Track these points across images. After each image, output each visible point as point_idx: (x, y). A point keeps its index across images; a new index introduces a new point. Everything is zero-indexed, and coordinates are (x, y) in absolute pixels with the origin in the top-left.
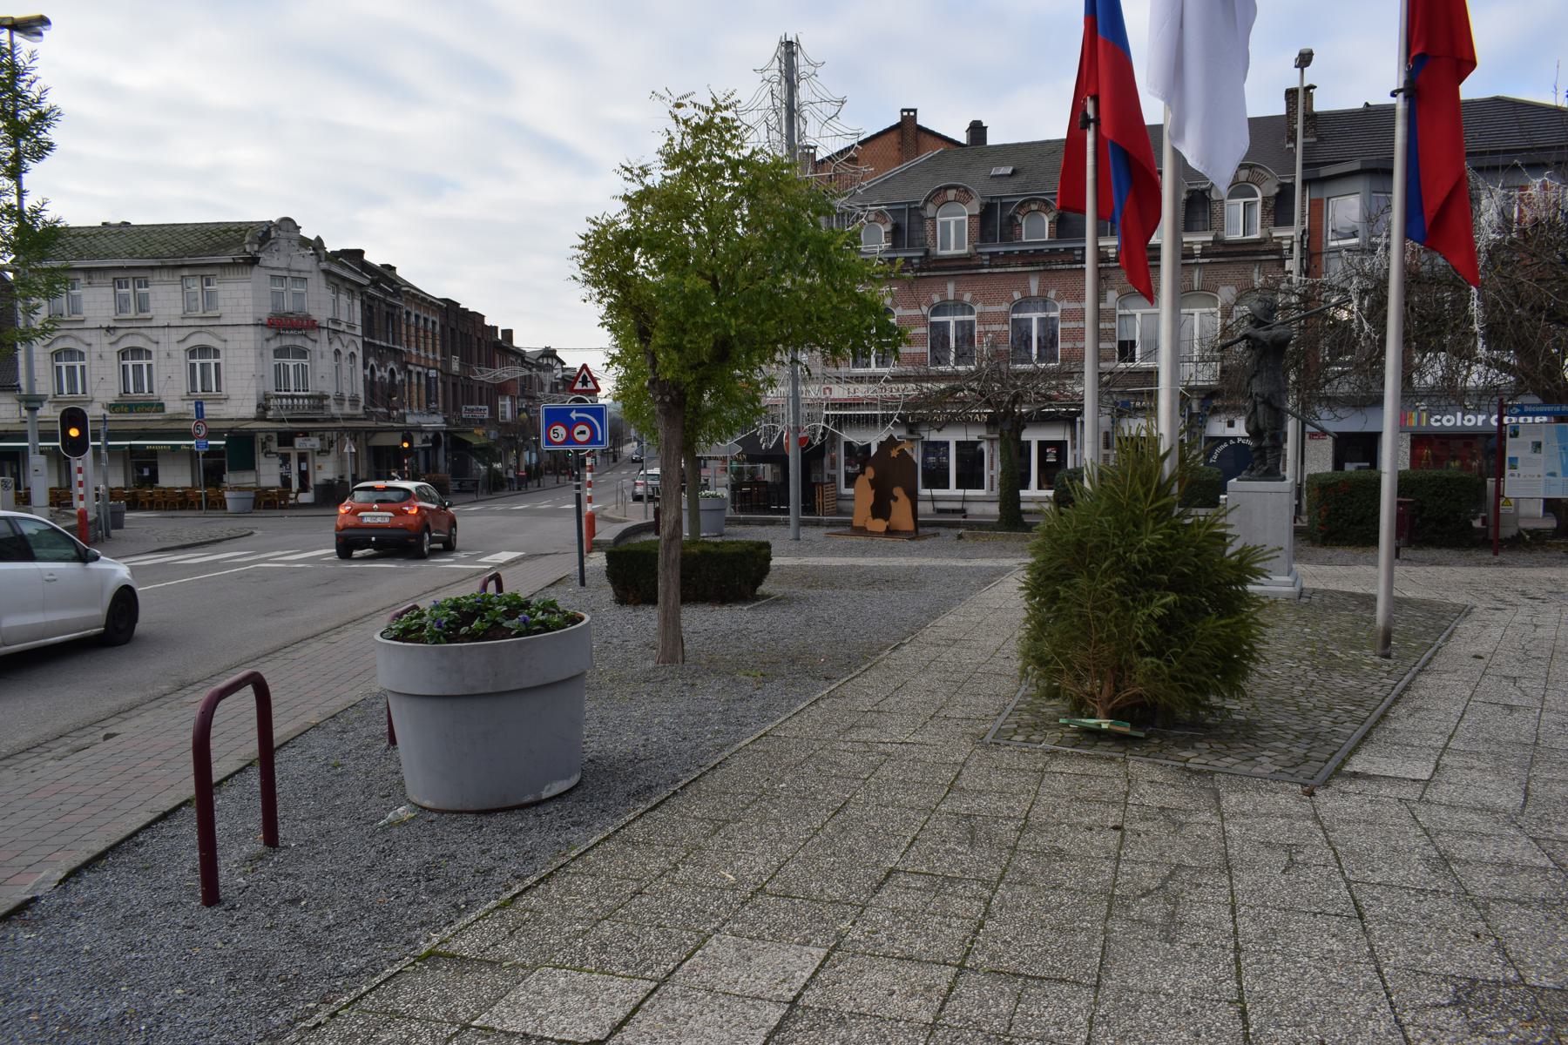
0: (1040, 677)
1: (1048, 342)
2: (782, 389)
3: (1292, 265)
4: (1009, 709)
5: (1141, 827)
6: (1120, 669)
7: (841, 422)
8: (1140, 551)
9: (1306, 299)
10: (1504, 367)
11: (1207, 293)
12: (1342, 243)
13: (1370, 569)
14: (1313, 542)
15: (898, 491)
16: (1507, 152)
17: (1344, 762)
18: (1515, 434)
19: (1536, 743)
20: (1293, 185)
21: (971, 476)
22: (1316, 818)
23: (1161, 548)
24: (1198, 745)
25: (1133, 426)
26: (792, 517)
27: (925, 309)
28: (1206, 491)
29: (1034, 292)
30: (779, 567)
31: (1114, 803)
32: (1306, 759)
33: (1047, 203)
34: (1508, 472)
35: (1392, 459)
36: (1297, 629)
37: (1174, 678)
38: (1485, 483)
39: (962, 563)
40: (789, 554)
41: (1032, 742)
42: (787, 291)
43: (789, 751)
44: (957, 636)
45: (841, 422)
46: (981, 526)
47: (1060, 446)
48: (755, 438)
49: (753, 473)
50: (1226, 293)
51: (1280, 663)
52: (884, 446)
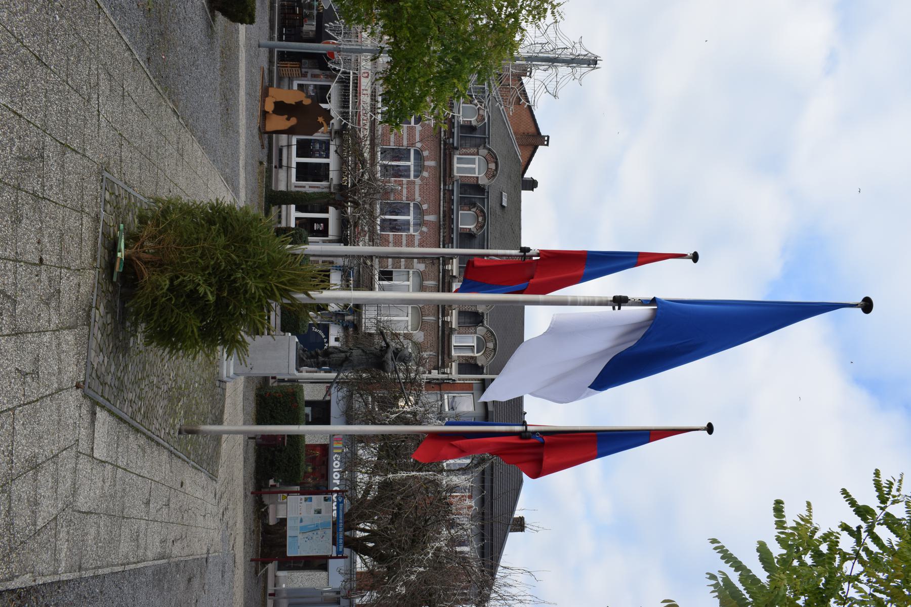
0: (154, 212)
1: (394, 226)
2: (369, 42)
3: (435, 374)
4: (130, 190)
5: (44, 276)
6: (161, 265)
7: (344, 83)
8: (243, 278)
9: (413, 382)
10: (367, 492)
11: (421, 324)
12: (446, 401)
13: (241, 422)
14: (259, 389)
15: (293, 121)
16: (492, 487)
17: (103, 407)
18: (326, 500)
19: (124, 518)
20: (482, 373)
21: (304, 172)
22: (59, 390)
23: (246, 292)
24: (109, 316)
25: (335, 278)
26: (276, 42)
27: (419, 145)
28: (292, 321)
29: (427, 218)
30: (237, 30)
31: (61, 259)
32: (104, 384)
33: (482, 227)
34: (303, 497)
35: (313, 433)
36: (197, 379)
37: (156, 299)
38: (297, 485)
39: (242, 163)
40: (248, 39)
41: (105, 205)
42: (428, 47)
43: (86, 25)
44: (185, 157)
45: (344, 83)
46: (269, 177)
47: (325, 233)
48: (334, 19)
49: (310, 17)
50: (419, 336)
51: (175, 368)
52: (327, 114)
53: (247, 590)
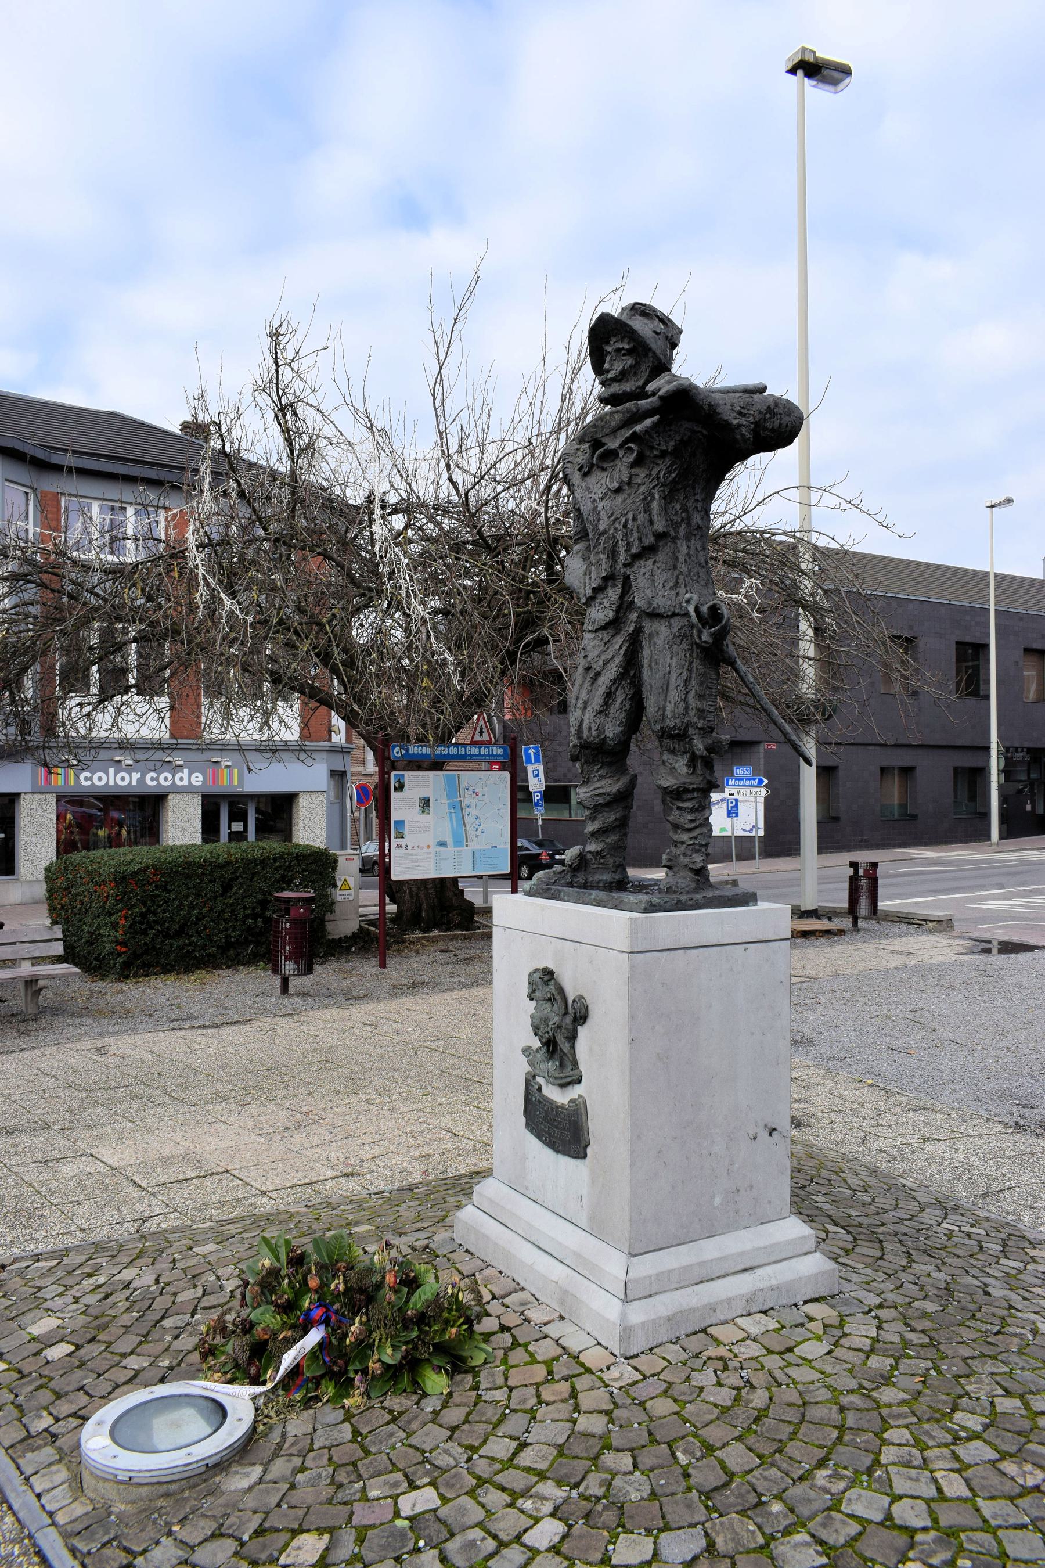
53: (900, 793)
